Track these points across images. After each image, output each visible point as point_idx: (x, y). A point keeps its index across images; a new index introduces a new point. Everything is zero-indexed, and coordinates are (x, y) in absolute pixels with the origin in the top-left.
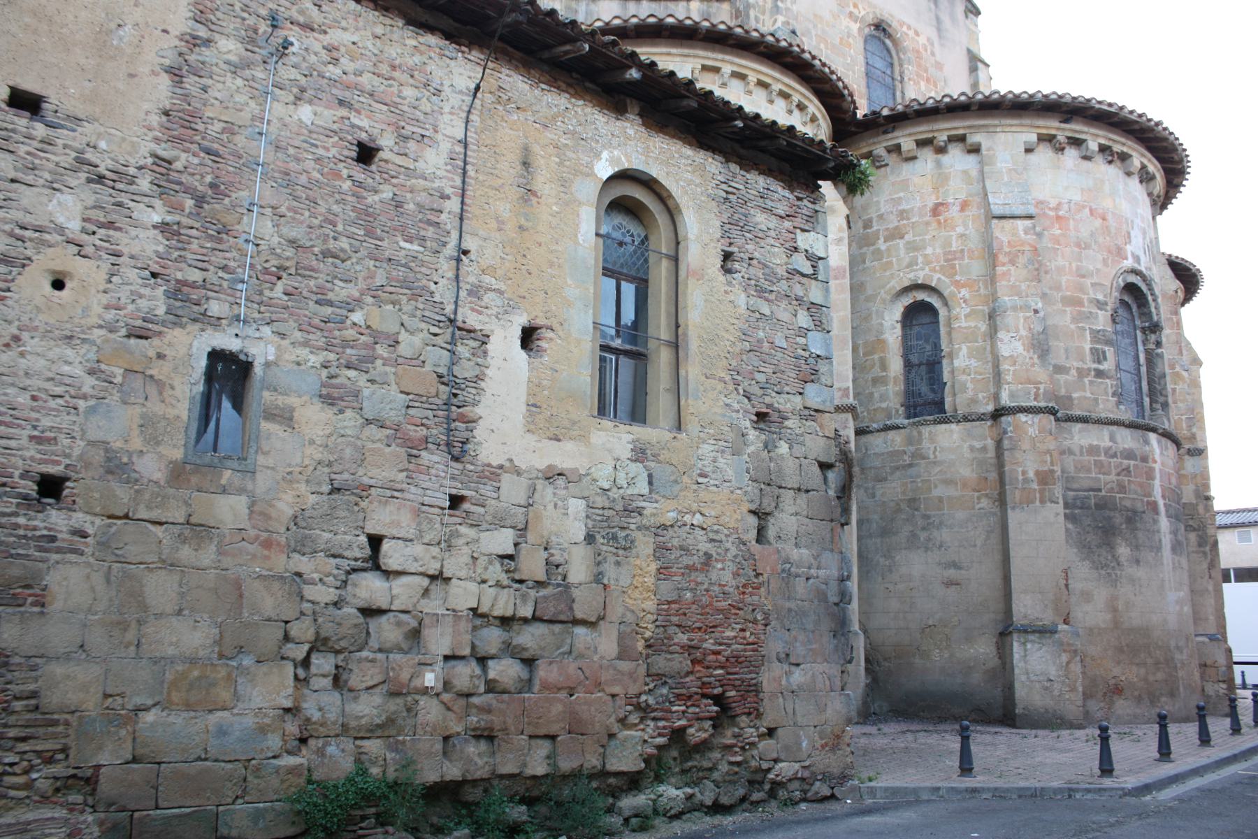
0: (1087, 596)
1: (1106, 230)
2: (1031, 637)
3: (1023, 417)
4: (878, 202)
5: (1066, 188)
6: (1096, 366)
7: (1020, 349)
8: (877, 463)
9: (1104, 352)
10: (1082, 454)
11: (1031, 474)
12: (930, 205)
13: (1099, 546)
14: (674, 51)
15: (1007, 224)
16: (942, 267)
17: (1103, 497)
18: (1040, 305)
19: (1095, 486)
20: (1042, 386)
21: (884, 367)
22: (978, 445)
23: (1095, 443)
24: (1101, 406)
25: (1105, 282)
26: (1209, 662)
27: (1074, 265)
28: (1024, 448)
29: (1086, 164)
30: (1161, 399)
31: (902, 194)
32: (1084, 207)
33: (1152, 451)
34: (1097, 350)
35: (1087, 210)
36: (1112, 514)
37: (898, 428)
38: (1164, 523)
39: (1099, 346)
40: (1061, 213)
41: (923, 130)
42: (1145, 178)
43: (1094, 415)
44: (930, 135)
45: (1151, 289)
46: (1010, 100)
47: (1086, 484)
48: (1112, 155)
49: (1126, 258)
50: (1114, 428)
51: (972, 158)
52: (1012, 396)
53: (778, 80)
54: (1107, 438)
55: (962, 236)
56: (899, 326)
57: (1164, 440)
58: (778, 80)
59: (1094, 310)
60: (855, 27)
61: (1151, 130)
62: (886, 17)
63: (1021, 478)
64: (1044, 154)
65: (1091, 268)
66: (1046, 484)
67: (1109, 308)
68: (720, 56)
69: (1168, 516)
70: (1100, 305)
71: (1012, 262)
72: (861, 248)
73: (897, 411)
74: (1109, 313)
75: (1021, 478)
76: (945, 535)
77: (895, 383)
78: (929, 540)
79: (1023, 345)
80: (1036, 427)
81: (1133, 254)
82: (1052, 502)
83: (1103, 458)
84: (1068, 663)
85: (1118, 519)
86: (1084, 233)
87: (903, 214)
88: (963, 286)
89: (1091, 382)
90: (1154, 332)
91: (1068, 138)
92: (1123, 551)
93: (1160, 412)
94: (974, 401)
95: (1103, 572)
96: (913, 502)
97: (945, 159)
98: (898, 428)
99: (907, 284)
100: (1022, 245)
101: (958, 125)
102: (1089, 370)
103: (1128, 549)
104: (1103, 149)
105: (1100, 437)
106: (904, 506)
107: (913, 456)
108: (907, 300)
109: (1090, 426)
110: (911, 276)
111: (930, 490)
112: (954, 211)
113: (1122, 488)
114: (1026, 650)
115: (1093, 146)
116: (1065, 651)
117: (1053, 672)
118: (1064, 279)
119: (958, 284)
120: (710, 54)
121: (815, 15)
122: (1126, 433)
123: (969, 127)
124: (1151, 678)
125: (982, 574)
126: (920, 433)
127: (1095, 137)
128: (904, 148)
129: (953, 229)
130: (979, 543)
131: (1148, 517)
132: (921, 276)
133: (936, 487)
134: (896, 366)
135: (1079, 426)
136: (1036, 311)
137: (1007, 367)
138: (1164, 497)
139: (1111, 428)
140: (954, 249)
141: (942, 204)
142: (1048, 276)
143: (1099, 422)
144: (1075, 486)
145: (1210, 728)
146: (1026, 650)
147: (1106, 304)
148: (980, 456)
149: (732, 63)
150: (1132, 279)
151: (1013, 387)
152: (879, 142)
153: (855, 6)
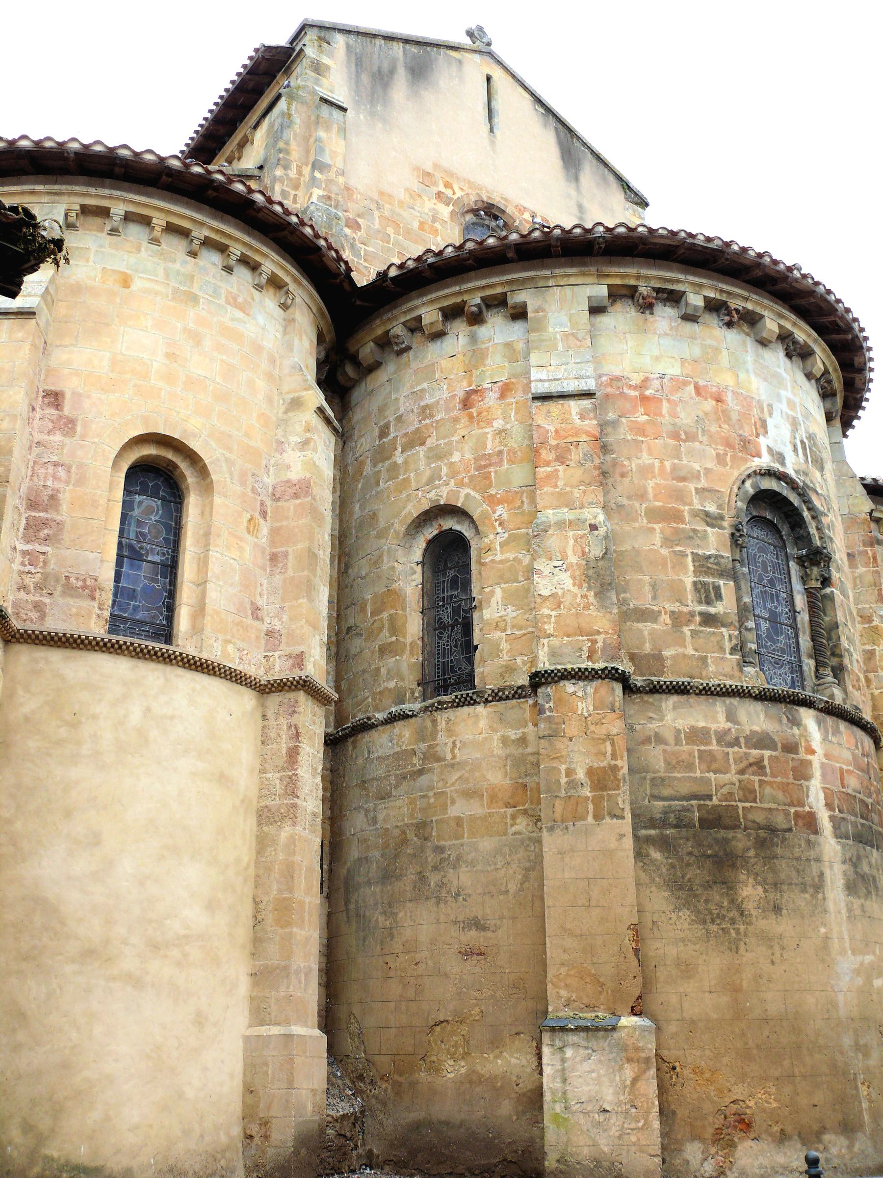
0: (686, 969)
1: (723, 415)
2: (572, 1038)
3: (569, 687)
4: (397, 399)
5: (657, 359)
6: (703, 608)
7: (568, 583)
8: (381, 772)
9: (717, 589)
10: (678, 741)
11: (581, 775)
12: (460, 394)
13: (707, 886)
14: (40, 188)
15: (554, 407)
16: (472, 478)
18: (601, 518)
19: (703, 790)
20: (600, 638)
21: (394, 630)
22: (513, 734)
23: (701, 724)
24: (712, 668)
25: (723, 484)
27: (668, 464)
28: (569, 734)
29: (689, 327)
30: (834, 661)
31: (425, 385)
32: (686, 384)
33: (805, 735)
34: (704, 584)
35: (691, 388)
36: (730, 834)
37: (404, 717)
38: (830, 846)
39: (708, 579)
40: (648, 393)
41: (450, 293)
42: (798, 352)
43: (696, 681)
44: (458, 300)
45: (807, 502)
46: (558, 239)
48: (729, 314)
49: (759, 455)
50: (735, 701)
51: (518, 327)
52: (553, 654)
53: (202, 224)
54: (721, 717)
55: (500, 432)
56: (419, 569)
57: (830, 721)
58: (202, 224)
59: (701, 527)
60: (445, 211)
61: (811, 293)
62: (496, 200)
63: (564, 780)
64: (622, 316)
65: (697, 466)
66: (604, 788)
67: (725, 524)
68: (106, 192)
69: (839, 834)
70: (712, 520)
71: (561, 459)
72: (375, 465)
73: (413, 693)
74: (727, 532)
75: (564, 780)
76: (463, 878)
77: (412, 653)
78: (442, 885)
79: (573, 577)
80: (590, 700)
81: (770, 450)
82: (614, 816)
83: (714, 747)
84: (635, 1080)
85: (741, 841)
86: (686, 418)
87: (426, 411)
88: (500, 502)
90: (817, 564)
91: (658, 291)
92: (750, 892)
93: (830, 679)
94: (510, 669)
95: (714, 928)
96: (422, 828)
97: (483, 331)
98: (404, 717)
99: (426, 506)
100: (576, 434)
101: (494, 283)
102: (692, 614)
103: (760, 889)
104: (785, 337)
105: (712, 716)
106: (411, 835)
107: (425, 757)
108: (431, 532)
109: (693, 699)
110: (432, 495)
111: (445, 808)
112: (491, 398)
113: (749, 794)
114: (563, 1060)
115: (696, 300)
116: (629, 1060)
117: (609, 1096)
118: (650, 484)
119: (493, 501)
120: (92, 190)
121: (381, 193)
122: (758, 708)
123: (510, 282)
124: (803, 1101)
125: (506, 937)
126: (434, 722)
127: (697, 291)
128: (426, 321)
129: (489, 423)
130: (512, 887)
131: (799, 837)
132: (443, 495)
133: (453, 802)
134: (414, 626)
135: (674, 698)
136: (593, 527)
137: (546, 611)
138: (829, 806)
139: (728, 700)
140: (489, 451)
141: (475, 391)
142: (626, 480)
143: (707, 692)
144: (666, 792)
146: (563, 1060)
147: (722, 518)
148: (517, 751)
149: (125, 201)
150: (769, 484)
151: (555, 642)
152: (395, 318)
153: (448, 185)
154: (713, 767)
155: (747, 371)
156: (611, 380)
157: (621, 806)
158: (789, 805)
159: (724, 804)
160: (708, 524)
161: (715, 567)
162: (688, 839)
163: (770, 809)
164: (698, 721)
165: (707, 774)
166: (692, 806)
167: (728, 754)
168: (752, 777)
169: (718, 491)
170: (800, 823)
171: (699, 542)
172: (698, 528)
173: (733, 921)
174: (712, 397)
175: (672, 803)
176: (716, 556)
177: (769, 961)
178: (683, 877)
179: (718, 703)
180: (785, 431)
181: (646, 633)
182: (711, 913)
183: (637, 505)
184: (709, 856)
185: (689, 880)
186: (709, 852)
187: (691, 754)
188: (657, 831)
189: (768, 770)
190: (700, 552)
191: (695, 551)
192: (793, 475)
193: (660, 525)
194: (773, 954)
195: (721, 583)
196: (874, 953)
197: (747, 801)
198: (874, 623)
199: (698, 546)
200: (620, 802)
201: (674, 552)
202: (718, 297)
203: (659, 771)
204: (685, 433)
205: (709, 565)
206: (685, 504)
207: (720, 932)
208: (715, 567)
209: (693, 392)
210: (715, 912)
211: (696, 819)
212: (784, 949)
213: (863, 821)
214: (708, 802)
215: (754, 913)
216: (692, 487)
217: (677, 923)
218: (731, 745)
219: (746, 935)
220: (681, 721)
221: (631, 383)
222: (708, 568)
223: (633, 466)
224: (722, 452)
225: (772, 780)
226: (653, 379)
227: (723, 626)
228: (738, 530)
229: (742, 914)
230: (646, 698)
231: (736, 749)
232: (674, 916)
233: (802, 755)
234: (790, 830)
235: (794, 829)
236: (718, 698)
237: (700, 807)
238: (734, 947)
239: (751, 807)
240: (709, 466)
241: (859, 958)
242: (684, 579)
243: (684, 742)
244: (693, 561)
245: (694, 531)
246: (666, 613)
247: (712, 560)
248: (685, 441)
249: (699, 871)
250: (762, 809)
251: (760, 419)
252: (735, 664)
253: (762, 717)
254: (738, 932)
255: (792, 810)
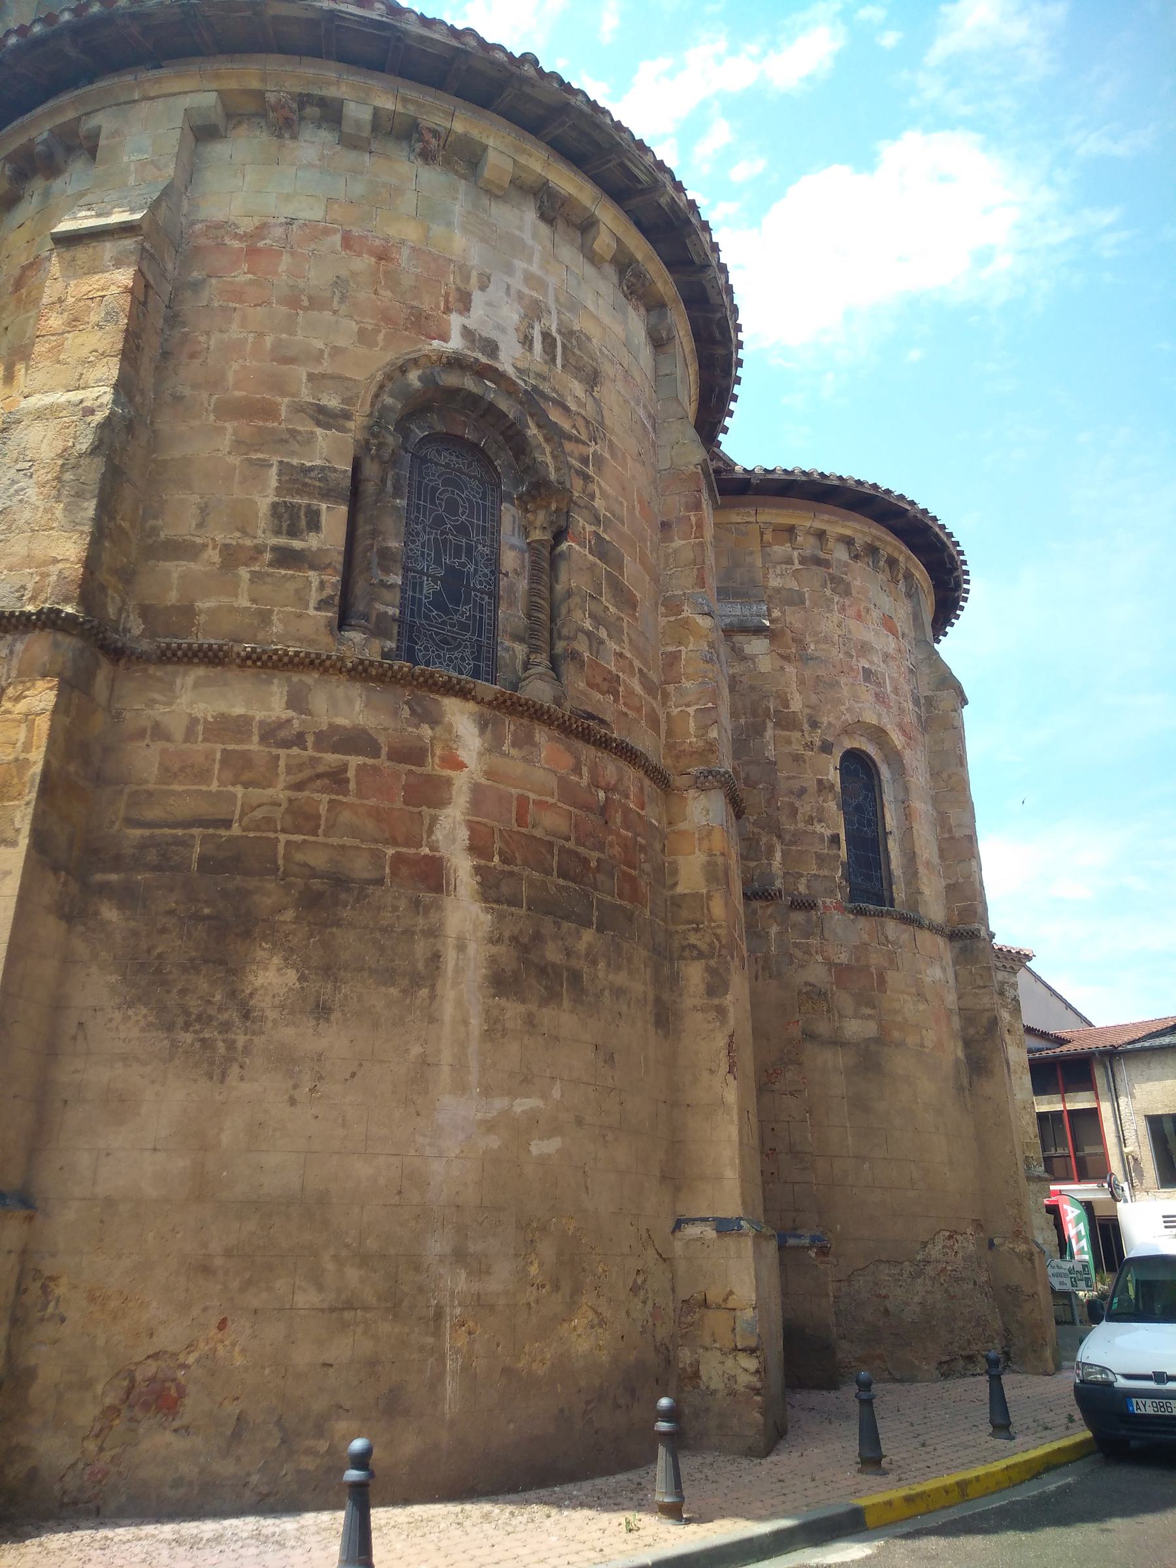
5: (288, 198)
6: (282, 541)
10: (190, 735)
17: (232, 840)
23: (239, 710)
24: (277, 628)
26: (714, 1296)
27: (269, 340)
29: (351, 158)
33: (452, 739)
35: (337, 239)
36: (252, 883)
38: (465, 915)
47: (185, 808)
59: (305, 426)
83: (254, 745)
85: (268, 896)
89: (256, 577)
92: (271, 977)
95: (188, 1037)
102: (259, 550)
103: (292, 976)
113: (303, 819)
122: (356, 691)
138: (476, 848)
144: (153, 813)
145: (1008, 1394)
147: (347, 416)
154: (247, 776)
155: (449, 224)
156: (208, 227)
157: (17, 825)
158: (386, 842)
159: (251, 835)
160: (319, 424)
161: (317, 484)
162: (172, 890)
163: (343, 847)
164: (233, 706)
165: (230, 788)
166: (192, 836)
167: (277, 757)
168: (316, 796)
169: (350, 379)
170: (404, 871)
171: (296, 447)
172: (299, 428)
173: (226, 1027)
174: (371, 253)
175: (157, 831)
176: (323, 469)
177: (286, 1097)
178: (149, 951)
179: (276, 681)
180: (511, 315)
181: (175, 575)
182: (187, 1013)
183: (205, 395)
184: (208, 917)
185: (160, 956)
186: (206, 911)
187: (209, 756)
188: (122, 875)
189: (352, 785)
190: (295, 462)
191: (285, 460)
192: (511, 372)
193: (236, 424)
194: (295, 1087)
195: (324, 506)
196: (544, 1096)
197: (298, 831)
198: (684, 614)
199: (293, 453)
200: (17, 820)
201: (249, 460)
202: (400, 109)
203: (147, 782)
204: (310, 298)
205: (307, 480)
206: (283, 394)
207: (198, 1045)
208: (317, 484)
209: (339, 243)
210: (195, 1011)
211: (195, 856)
212: (321, 1078)
213: (561, 882)
214: (223, 832)
215: (271, 1015)
216: (302, 372)
217: (121, 1027)
218: (286, 744)
219: (246, 1051)
220: (202, 706)
221: (238, 231)
222: (305, 485)
223: (212, 342)
224: (369, 327)
225: (357, 801)
226: (275, 225)
227: (312, 567)
228: (375, 436)
229: (246, 1016)
230: (152, 670)
231: (295, 750)
232: (118, 1016)
233: (433, 766)
234: (380, 882)
235: (388, 881)
236: (276, 672)
237: (205, 839)
238: (218, 1072)
239: (304, 841)
240: (341, 343)
241: (500, 1103)
242: (257, 498)
243: (200, 738)
244: (280, 474)
245: (293, 433)
246: (214, 549)
247: (313, 474)
248: (306, 309)
249: (179, 942)
250: (326, 845)
251: (458, 289)
252: (323, 622)
253: (358, 705)
254: (231, 1045)
255: (390, 851)
